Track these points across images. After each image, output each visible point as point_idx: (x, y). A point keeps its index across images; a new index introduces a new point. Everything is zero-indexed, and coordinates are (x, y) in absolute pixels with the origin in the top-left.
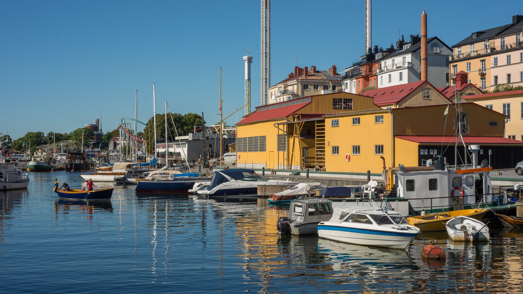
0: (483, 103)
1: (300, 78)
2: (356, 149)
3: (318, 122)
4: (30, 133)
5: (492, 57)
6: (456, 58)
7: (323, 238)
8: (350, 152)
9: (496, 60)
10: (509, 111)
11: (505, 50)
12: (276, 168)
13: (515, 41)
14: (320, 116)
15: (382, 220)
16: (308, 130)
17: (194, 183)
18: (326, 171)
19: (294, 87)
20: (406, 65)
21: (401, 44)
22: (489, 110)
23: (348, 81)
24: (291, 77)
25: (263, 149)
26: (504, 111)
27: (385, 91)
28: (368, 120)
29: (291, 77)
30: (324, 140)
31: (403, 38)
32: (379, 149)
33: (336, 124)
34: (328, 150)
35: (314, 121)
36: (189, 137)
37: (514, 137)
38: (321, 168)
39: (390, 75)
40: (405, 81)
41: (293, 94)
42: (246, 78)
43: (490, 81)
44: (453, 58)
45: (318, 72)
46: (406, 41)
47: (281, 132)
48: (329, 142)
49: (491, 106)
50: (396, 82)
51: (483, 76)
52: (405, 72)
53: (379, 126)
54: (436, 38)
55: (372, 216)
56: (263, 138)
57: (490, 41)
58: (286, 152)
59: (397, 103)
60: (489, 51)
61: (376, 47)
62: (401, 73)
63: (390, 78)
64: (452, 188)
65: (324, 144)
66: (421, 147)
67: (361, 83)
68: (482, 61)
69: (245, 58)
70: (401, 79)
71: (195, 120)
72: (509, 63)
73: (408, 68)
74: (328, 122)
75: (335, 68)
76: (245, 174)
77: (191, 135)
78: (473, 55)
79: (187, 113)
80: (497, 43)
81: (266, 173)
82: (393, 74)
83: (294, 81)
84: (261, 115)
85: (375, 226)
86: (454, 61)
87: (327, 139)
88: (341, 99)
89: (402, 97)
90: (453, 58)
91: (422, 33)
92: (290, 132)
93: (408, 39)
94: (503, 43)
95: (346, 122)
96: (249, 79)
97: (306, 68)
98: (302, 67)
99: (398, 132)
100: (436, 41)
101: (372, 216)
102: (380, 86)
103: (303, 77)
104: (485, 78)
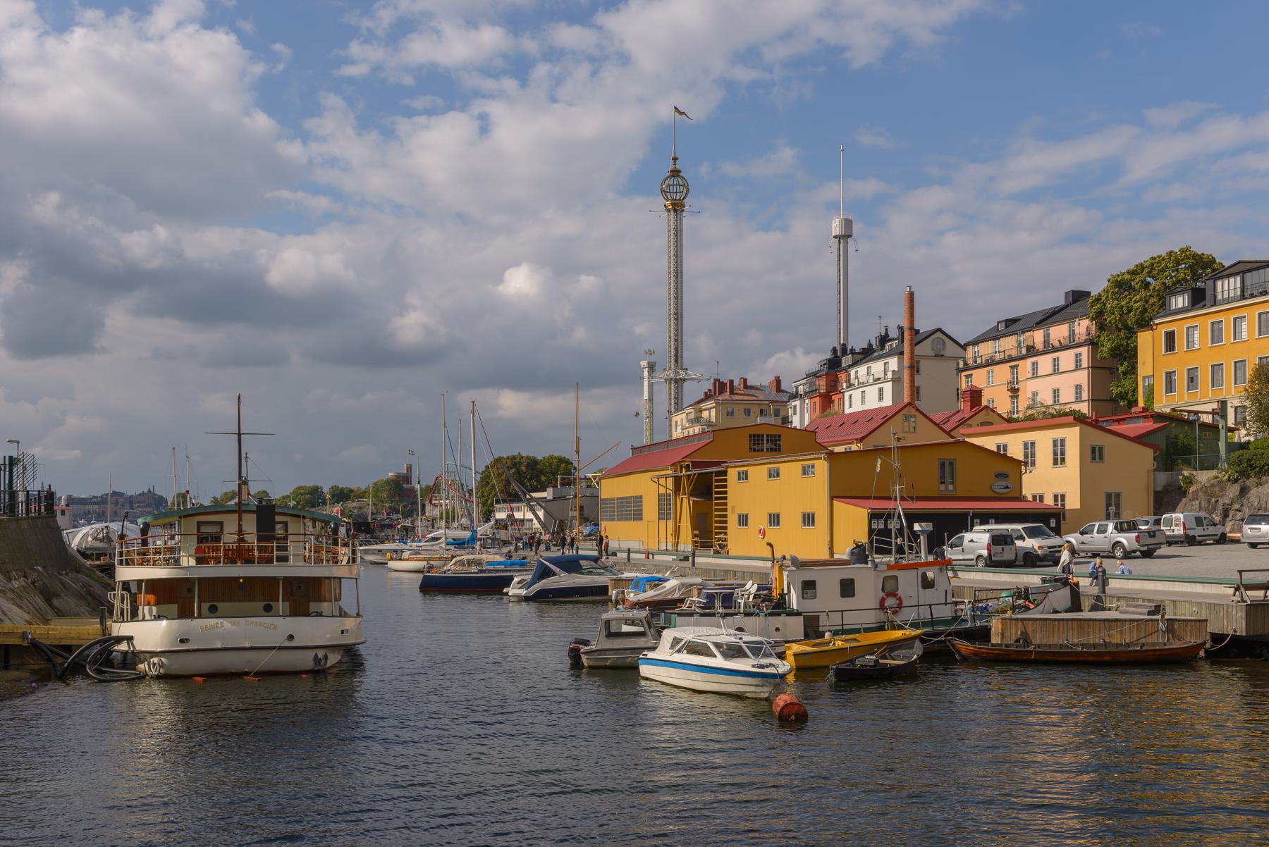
0: (990, 443)
1: (721, 398)
2: (775, 519)
3: (718, 473)
4: (300, 488)
5: (1030, 361)
6: (971, 362)
7: (647, 679)
8: (764, 523)
10: (1033, 455)
11: (1049, 349)
12: (653, 547)
13: (1066, 334)
15: (733, 651)
16: (703, 486)
17: (512, 578)
18: (731, 553)
19: (710, 413)
20: (890, 375)
21: (884, 339)
22: (1000, 455)
23: (797, 403)
24: (708, 397)
25: (638, 516)
26: (1026, 456)
28: (790, 469)
29: (708, 397)
30: (726, 504)
32: (809, 519)
33: (743, 476)
34: (732, 520)
36: (548, 494)
37: (1041, 497)
38: (722, 550)
41: (709, 424)
42: (646, 396)
43: (1023, 403)
44: (966, 364)
45: (752, 387)
47: (662, 491)
48: (733, 508)
49: (1005, 447)
50: (872, 403)
51: (1014, 392)
52: (888, 387)
53: (808, 480)
54: (940, 330)
55: (718, 645)
56: (639, 499)
58: (670, 523)
59: (861, 440)
60: (1024, 351)
62: (881, 390)
63: (863, 397)
64: (882, 594)
65: (726, 510)
66: (873, 516)
67: (817, 405)
68: (1012, 367)
69: (644, 363)
70: (881, 399)
71: (559, 466)
72: (1056, 371)
73: (893, 380)
74: (732, 474)
75: (778, 381)
76: (583, 563)
77: (550, 490)
78: (998, 357)
79: (546, 455)
80: (1038, 336)
81: (632, 556)
82: (870, 391)
83: (711, 403)
84: (642, 458)
85: (719, 661)
86: (967, 367)
87: (731, 502)
89: (870, 429)
90: (966, 364)
91: (905, 325)
92: (677, 489)
93: (894, 333)
94: (1047, 336)
95: (758, 472)
96: (651, 399)
97: (731, 382)
99: (838, 493)
100: (939, 334)
101: (718, 645)
102: (847, 411)
103: (726, 396)
104: (1017, 397)
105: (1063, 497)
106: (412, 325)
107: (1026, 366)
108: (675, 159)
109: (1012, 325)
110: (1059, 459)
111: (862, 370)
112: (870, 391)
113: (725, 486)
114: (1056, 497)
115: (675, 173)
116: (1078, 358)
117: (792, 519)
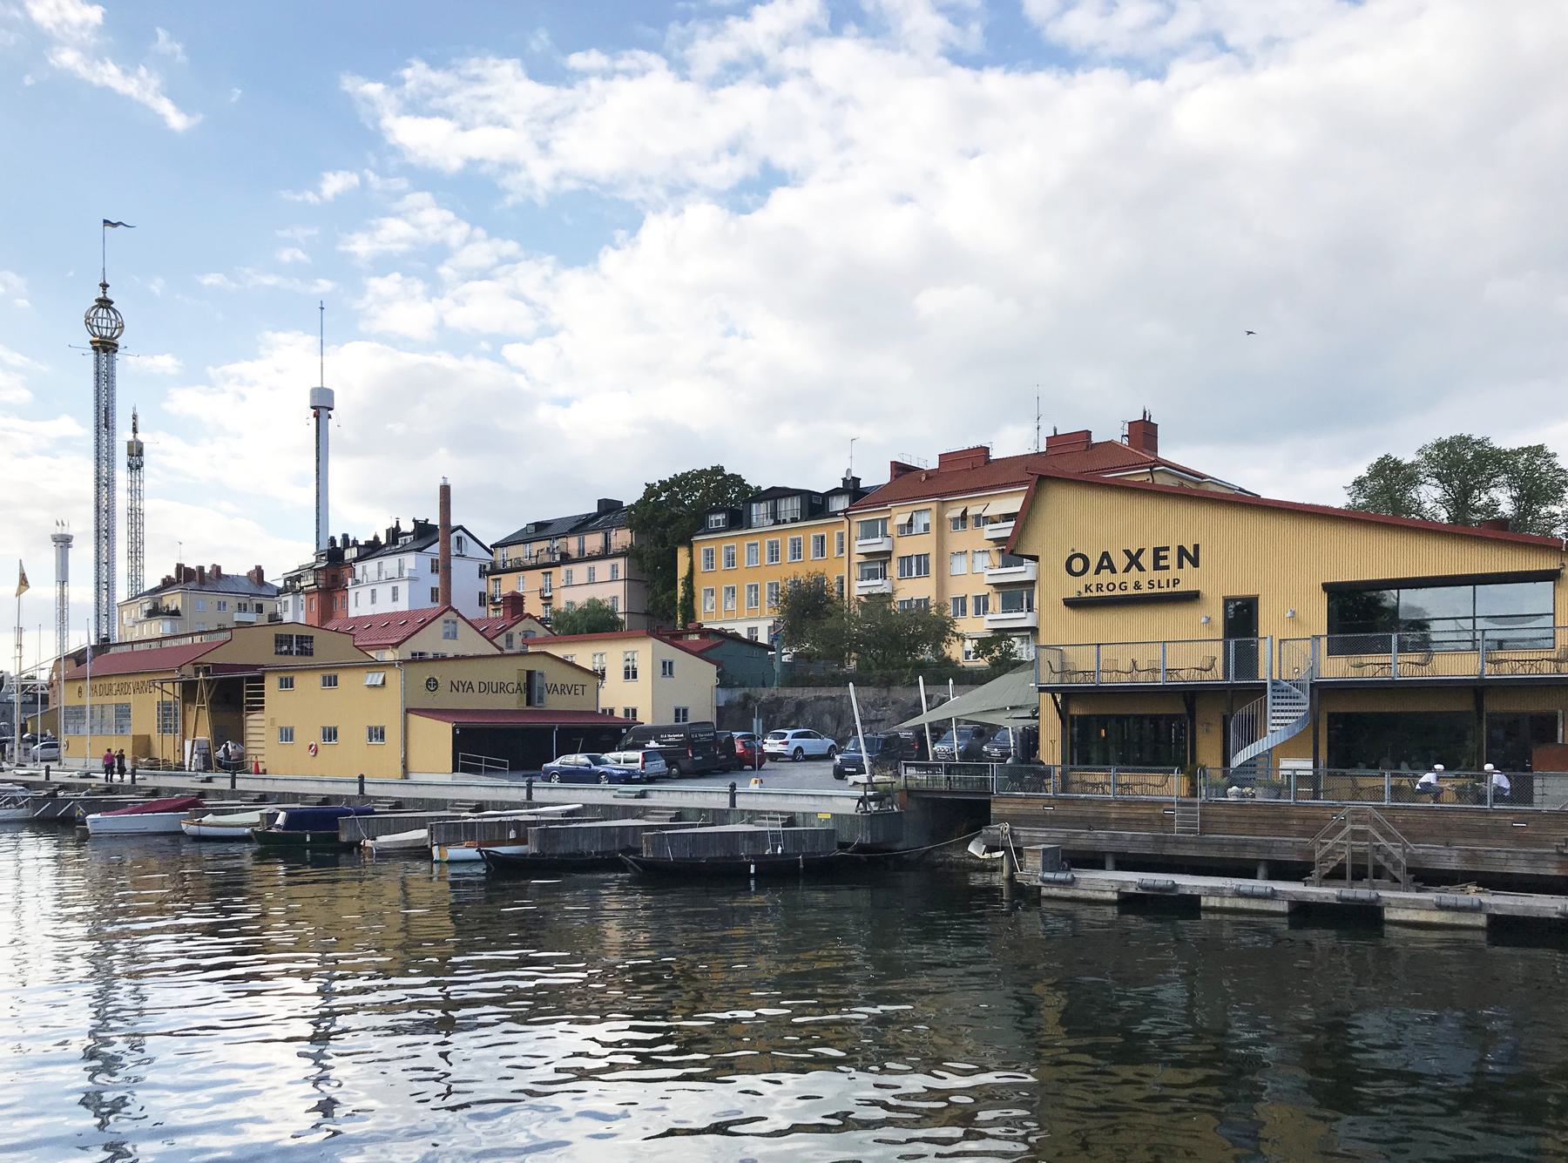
2: (331, 734)
3: (250, 679)
5: (564, 568)
8: (317, 738)
9: (569, 573)
11: (584, 558)
14: (254, 667)
21: (395, 534)
23: (290, 598)
27: (371, 622)
32: (377, 734)
33: (287, 684)
37: (612, 711)
39: (373, 591)
40: (403, 605)
46: (403, 529)
47: (167, 698)
50: (385, 606)
52: (404, 588)
54: (461, 527)
60: (558, 558)
61: (345, 537)
62: (395, 589)
70: (395, 598)
74: (271, 683)
80: (572, 544)
95: (309, 684)
100: (460, 533)
105: (634, 711)
106: (397, 276)
107: (560, 573)
108: (105, 286)
109: (541, 530)
110: (631, 673)
111: (371, 565)
112: (376, 594)
113: (262, 695)
114: (627, 711)
115: (105, 303)
116: (614, 569)
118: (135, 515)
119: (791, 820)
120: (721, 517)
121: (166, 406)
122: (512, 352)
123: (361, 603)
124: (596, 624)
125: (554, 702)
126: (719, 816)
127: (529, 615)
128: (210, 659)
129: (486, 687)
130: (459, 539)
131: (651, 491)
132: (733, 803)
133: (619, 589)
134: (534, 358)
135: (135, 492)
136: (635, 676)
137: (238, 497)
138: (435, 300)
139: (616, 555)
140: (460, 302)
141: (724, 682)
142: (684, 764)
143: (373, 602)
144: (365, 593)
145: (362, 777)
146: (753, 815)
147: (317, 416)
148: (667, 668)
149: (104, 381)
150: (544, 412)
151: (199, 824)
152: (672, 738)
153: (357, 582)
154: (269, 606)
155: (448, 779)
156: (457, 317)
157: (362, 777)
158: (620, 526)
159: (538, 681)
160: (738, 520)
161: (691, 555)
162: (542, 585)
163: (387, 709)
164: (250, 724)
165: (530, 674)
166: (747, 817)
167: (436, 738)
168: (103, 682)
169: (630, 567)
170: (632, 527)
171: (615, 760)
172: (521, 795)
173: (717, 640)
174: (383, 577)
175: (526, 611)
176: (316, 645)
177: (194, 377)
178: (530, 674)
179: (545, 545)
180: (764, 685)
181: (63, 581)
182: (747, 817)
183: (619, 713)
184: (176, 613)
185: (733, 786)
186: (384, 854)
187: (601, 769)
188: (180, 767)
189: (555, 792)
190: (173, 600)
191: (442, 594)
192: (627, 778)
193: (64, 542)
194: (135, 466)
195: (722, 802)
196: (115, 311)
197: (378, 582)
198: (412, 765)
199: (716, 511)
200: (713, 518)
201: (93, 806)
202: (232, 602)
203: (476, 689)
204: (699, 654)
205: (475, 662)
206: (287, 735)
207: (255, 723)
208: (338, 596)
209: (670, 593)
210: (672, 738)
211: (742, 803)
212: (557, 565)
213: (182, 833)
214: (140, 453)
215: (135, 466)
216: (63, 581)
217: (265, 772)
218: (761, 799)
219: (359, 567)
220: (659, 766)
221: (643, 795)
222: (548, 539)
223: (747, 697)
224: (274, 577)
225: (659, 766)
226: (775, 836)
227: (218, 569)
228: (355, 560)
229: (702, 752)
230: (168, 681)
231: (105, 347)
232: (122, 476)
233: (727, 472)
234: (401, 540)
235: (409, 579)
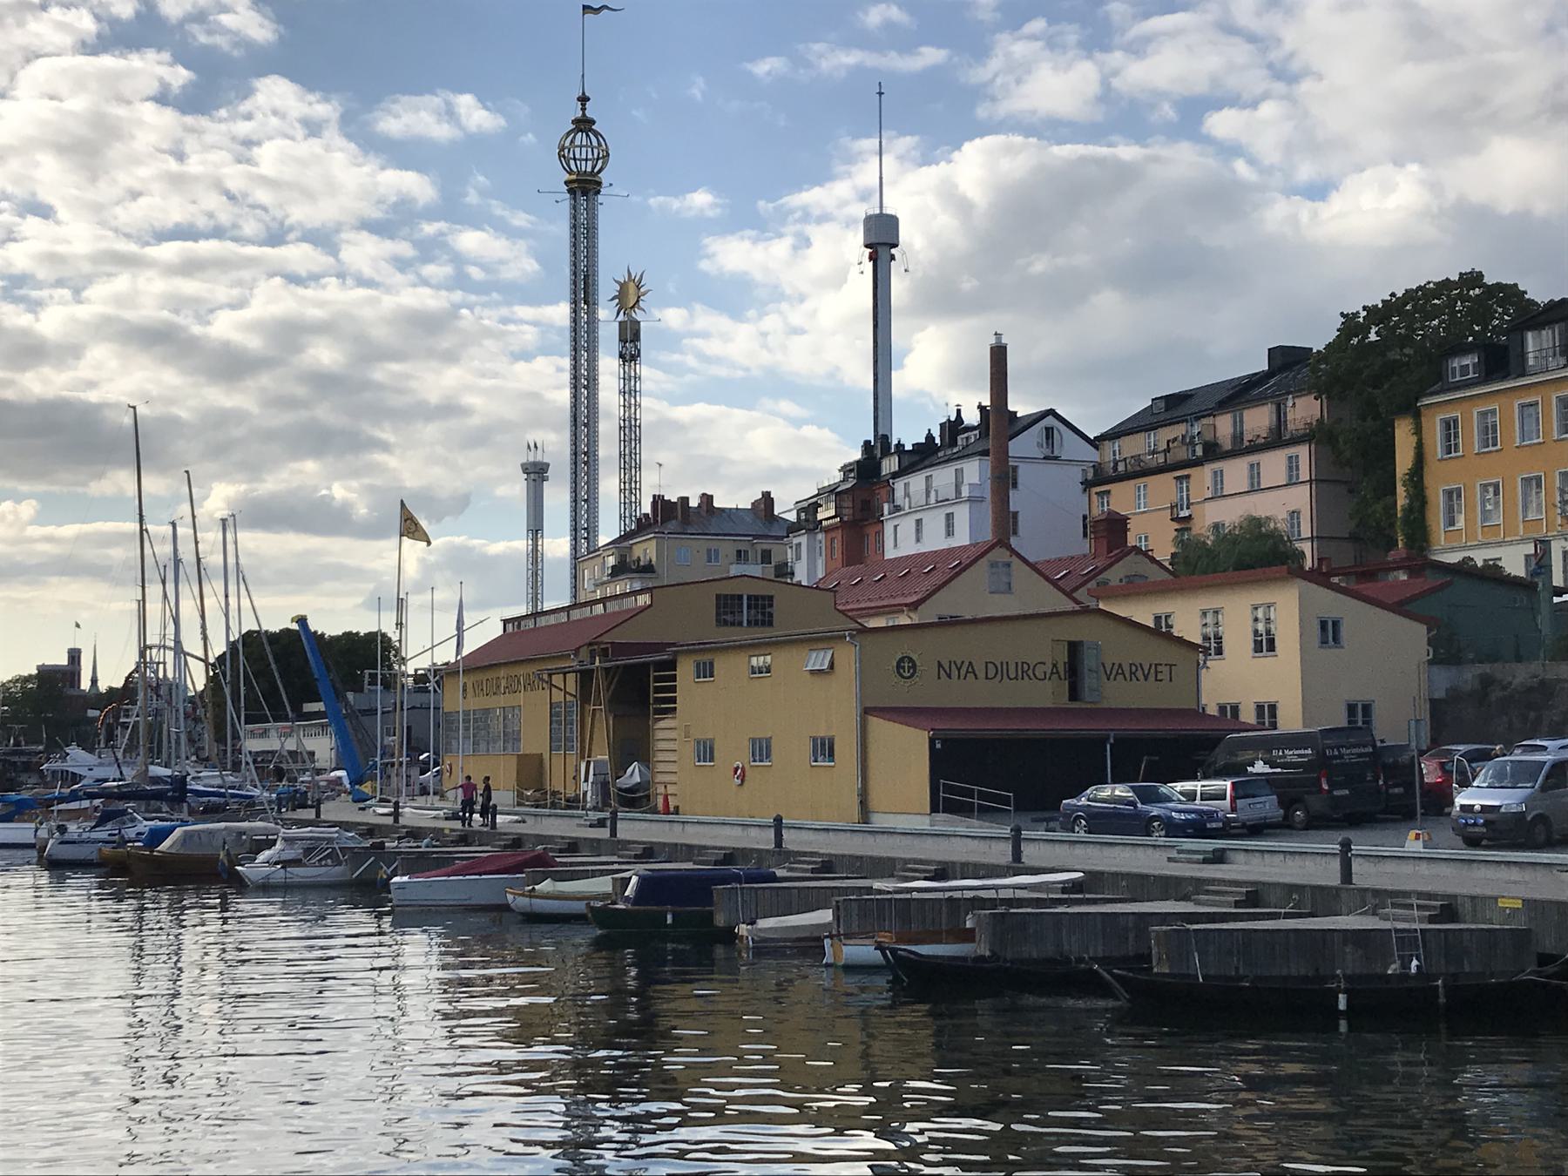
2: (762, 749)
3: (661, 666)
5: (1208, 470)
8: (742, 758)
11: (1242, 448)
23: (803, 540)
31: (959, 412)
32: (824, 748)
33: (705, 671)
35: (646, 665)
37: (1235, 709)
39: (919, 522)
40: (962, 538)
47: (558, 696)
50: (935, 540)
52: (962, 514)
54: (1051, 412)
57: (1204, 421)
60: (1199, 451)
62: (949, 517)
63: (919, 530)
67: (837, 545)
70: (950, 532)
74: (685, 670)
80: (1224, 426)
88: (740, 597)
92: (585, 695)
98: (672, 497)
100: (1050, 421)
107: (1203, 476)
108: (584, 100)
109: (1174, 407)
110: (1265, 644)
111: (917, 481)
114: (1260, 708)
115: (584, 124)
116: (1292, 464)
117: (793, 750)
118: (630, 431)
119: (1449, 909)
120: (1469, 360)
121: (704, 265)
122: (1222, 123)
123: (901, 539)
124: (1255, 556)
125: (1119, 694)
126: (1321, 899)
127: (1137, 550)
128: (619, 637)
129: (999, 671)
130: (1049, 431)
131: (1350, 325)
132: (1347, 874)
133: (1300, 498)
134: (1259, 128)
135: (629, 390)
136: (1271, 646)
137: (763, 390)
138: (1098, 55)
139: (1295, 441)
140: (1138, 49)
141: (1445, 652)
142: (1316, 803)
143: (918, 540)
144: (907, 525)
145: (778, 820)
146: (1378, 899)
147: (873, 258)
148: (1329, 632)
149: (584, 237)
150: (1277, 214)
151: (532, 894)
152: (1291, 755)
153: (898, 508)
154: (776, 550)
155: (923, 823)
156: (1139, 74)
157: (778, 820)
158: (1299, 392)
159: (1088, 661)
160: (1501, 362)
161: (1418, 431)
162: (1175, 498)
163: (836, 708)
164: (660, 735)
165: (1074, 648)
166: (1371, 901)
167: (905, 755)
168: (490, 675)
169: (1317, 461)
170: (1319, 390)
171: (1187, 793)
172: (1000, 853)
173: (1442, 579)
174: (932, 500)
175: (1131, 541)
176: (777, 610)
177: (745, 218)
178: (1074, 648)
179: (1178, 430)
180: (1519, 659)
181: (536, 529)
182: (1371, 901)
183: (1248, 716)
184: (649, 569)
185: (1346, 845)
186: (767, 948)
187: (1155, 810)
188: (574, 803)
189: (1079, 851)
190: (646, 549)
191: (1006, 523)
192: (1199, 827)
193: (536, 473)
194: (630, 354)
195: (1327, 873)
196: (597, 134)
197: (927, 507)
198: (875, 799)
199: (1464, 350)
200: (1456, 363)
201: (417, 863)
202: (727, 548)
203: (981, 675)
204: (1400, 608)
205: (985, 627)
206: (706, 751)
207: (667, 734)
208: (871, 531)
209: (1389, 499)
210: (1291, 755)
211: (1366, 875)
212: (1198, 463)
213: (506, 908)
214: (636, 337)
215: (630, 354)
216: (536, 529)
217: (677, 812)
218: (1424, 868)
219: (899, 486)
220: (1267, 806)
221: (1219, 857)
222: (1188, 425)
223: (1487, 682)
224: (785, 508)
225: (1267, 806)
226: (1407, 940)
227: (707, 499)
228: (895, 475)
229: (1351, 782)
230: (558, 671)
231: (584, 187)
232: (608, 366)
233: (1489, 280)
234: (961, 439)
235: (970, 500)
